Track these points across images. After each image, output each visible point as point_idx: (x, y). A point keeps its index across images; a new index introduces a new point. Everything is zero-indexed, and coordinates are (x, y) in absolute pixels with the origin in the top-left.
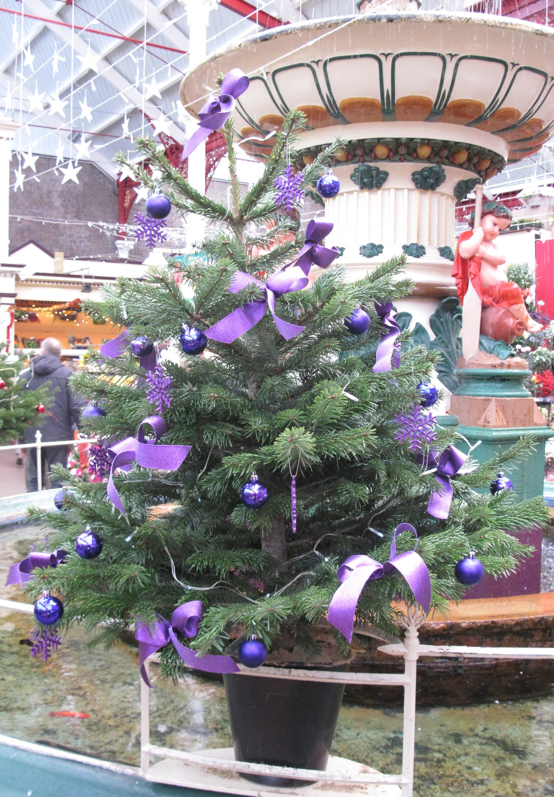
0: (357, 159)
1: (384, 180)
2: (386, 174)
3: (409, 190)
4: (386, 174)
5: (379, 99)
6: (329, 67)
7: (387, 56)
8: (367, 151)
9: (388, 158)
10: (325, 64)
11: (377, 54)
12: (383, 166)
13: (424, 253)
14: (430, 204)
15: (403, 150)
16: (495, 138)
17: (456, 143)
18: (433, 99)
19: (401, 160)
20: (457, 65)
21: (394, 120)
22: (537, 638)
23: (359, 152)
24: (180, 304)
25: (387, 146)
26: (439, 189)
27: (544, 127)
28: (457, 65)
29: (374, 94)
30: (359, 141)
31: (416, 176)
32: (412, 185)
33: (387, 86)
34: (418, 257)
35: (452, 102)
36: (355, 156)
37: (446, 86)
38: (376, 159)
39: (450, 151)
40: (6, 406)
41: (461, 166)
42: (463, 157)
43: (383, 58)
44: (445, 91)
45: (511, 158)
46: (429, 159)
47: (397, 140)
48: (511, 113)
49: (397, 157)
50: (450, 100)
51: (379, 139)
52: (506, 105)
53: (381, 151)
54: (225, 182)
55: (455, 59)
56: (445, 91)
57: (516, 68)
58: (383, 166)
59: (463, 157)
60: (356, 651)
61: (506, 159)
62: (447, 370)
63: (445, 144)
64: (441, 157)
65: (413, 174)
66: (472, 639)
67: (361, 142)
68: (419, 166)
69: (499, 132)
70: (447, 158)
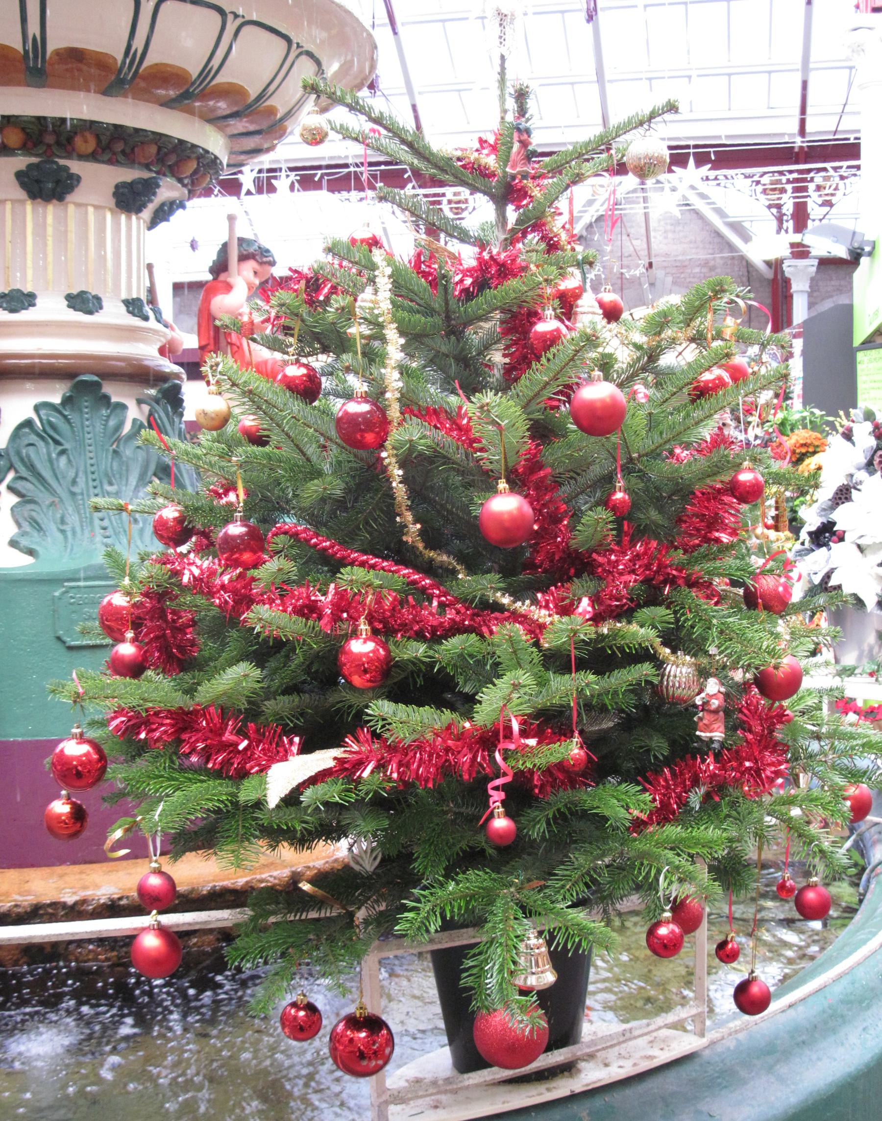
0: (41, 149)
2: (78, 179)
3: (13, 201)
4: (78, 179)
5: (120, 57)
8: (63, 139)
9: (93, 157)
12: (75, 166)
13: (34, 305)
14: (129, 229)
15: (119, 147)
16: (209, 129)
17: (137, 131)
18: (194, 72)
19: (110, 162)
20: (297, 57)
21: (43, 86)
23: (50, 139)
25: (23, 129)
26: (69, 198)
27: (279, 116)
28: (297, 57)
30: (181, 142)
32: (21, 194)
33: (138, 44)
34: (90, 313)
35: (151, 67)
37: (216, 62)
39: (126, 143)
44: (136, 51)
45: (232, 162)
46: (147, 167)
47: (41, 120)
49: (106, 157)
50: (146, 64)
56: (136, 51)
58: (75, 166)
60: (227, 734)
61: (225, 163)
63: (118, 130)
64: (114, 154)
66: (213, 904)
68: (128, 175)
70: (123, 152)
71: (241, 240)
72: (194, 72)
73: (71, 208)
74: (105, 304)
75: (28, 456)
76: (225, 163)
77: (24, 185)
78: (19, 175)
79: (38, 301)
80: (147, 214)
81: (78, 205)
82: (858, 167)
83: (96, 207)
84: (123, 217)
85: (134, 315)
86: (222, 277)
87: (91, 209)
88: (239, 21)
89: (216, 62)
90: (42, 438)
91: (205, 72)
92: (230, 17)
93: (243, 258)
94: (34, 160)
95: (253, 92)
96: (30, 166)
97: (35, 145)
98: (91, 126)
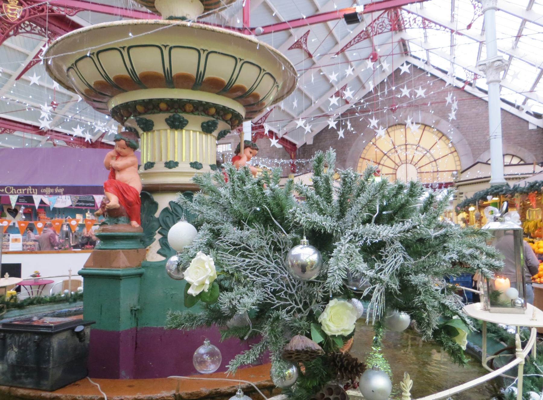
1: (186, 124)
3: (200, 132)
4: (187, 122)
6: (173, 51)
7: (204, 51)
9: (192, 112)
10: (171, 49)
11: (199, 49)
12: (186, 116)
18: (226, 81)
22: (48, 344)
24: (503, 339)
29: (193, 72)
31: (205, 125)
32: (167, 127)
33: (202, 69)
36: (149, 109)
37: (234, 77)
38: (185, 111)
40: (397, 393)
41: (226, 121)
42: (229, 116)
43: (163, 48)
46: (213, 116)
48: (240, 88)
49: (196, 113)
51: (161, 99)
52: (237, 83)
53: (189, 107)
54: (527, 283)
55: (265, 72)
57: (242, 62)
59: (229, 116)
62: (93, 205)
65: (202, 124)
67: (151, 100)
68: (206, 119)
69: (237, 99)
71: (245, 141)
72: (226, 81)
73: (184, 131)
74: (203, 166)
75: (166, 221)
76: (244, 116)
77: (168, 124)
78: (166, 120)
79: (179, 165)
80: (215, 133)
81: (186, 130)
82: (504, 175)
83: (194, 131)
84: (204, 136)
85: (193, 168)
86: (239, 155)
87: (191, 132)
88: (242, 62)
89: (234, 77)
90: (171, 214)
91: (250, 89)
92: (238, 61)
93: (246, 147)
94: (171, 114)
95: (248, 88)
96: (170, 117)
97: (172, 109)
98: (190, 101)
